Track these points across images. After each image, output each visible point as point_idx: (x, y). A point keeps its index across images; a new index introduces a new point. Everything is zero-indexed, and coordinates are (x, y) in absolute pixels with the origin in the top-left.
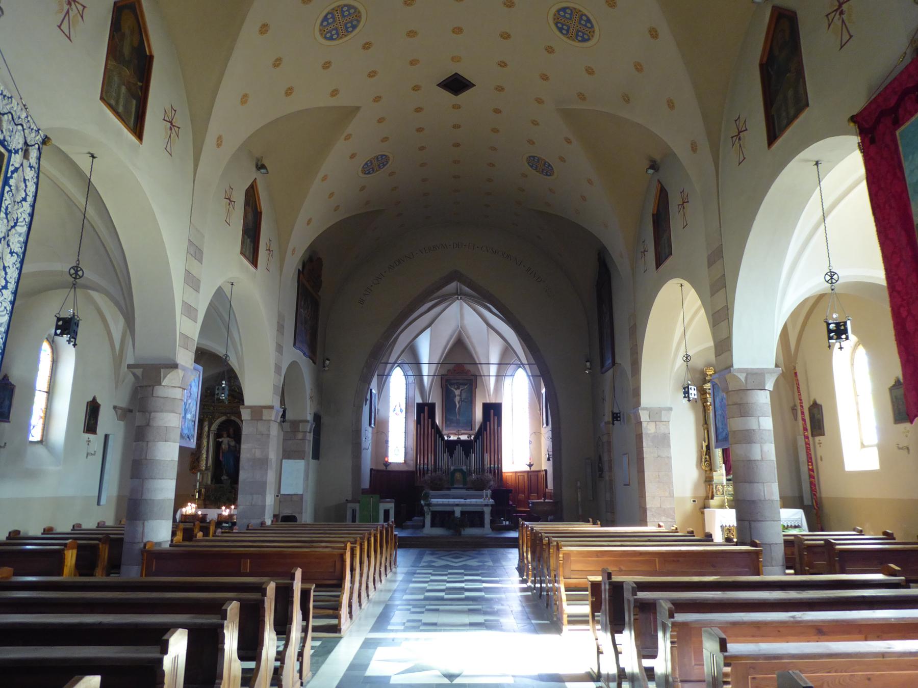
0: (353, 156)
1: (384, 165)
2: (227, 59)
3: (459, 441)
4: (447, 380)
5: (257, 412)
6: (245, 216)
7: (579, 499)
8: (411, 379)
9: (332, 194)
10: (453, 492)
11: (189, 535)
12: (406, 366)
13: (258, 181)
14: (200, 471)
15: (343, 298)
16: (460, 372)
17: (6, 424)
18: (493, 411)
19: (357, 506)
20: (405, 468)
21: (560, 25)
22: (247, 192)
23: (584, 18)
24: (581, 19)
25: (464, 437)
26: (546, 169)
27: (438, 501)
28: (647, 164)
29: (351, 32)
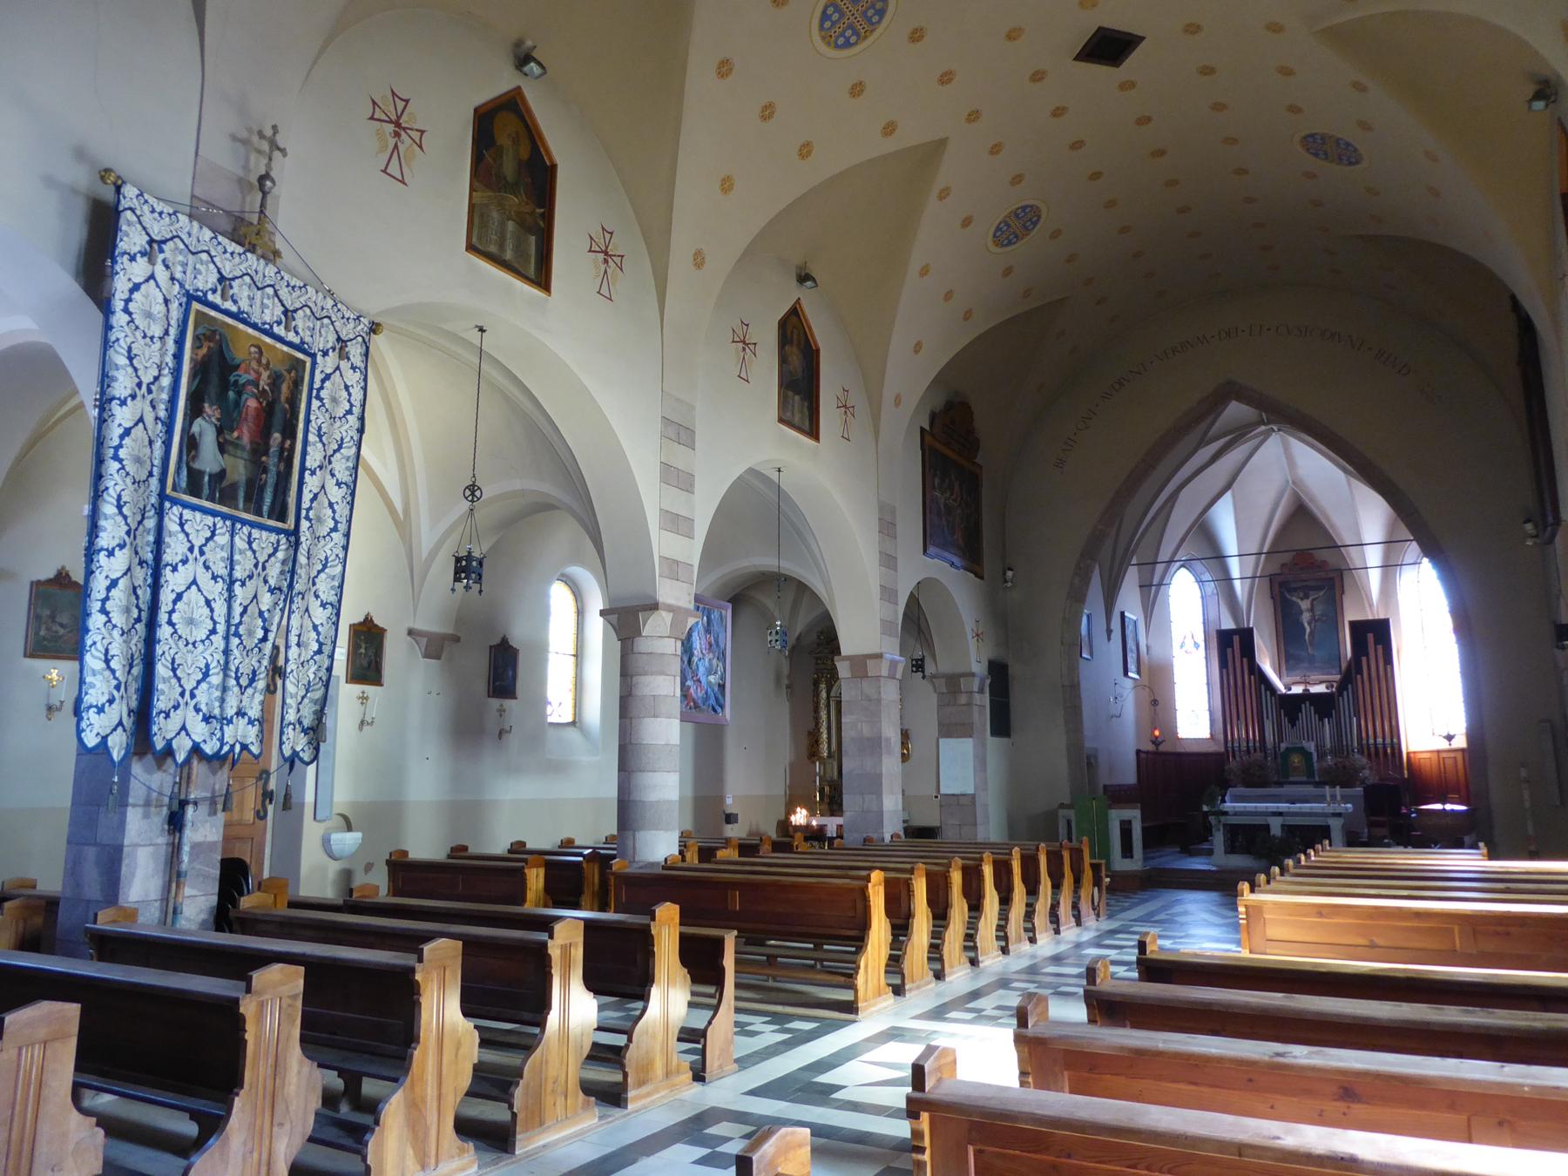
1: (1035, 224)
3: (1306, 696)
4: (1281, 585)
5: (860, 663)
6: (783, 360)
7: (1527, 804)
8: (1210, 587)
10: (1287, 790)
11: (706, 854)
12: (1198, 565)
13: (803, 302)
14: (821, 759)
15: (1022, 463)
16: (1304, 569)
17: (513, 702)
18: (1375, 636)
19: (1071, 814)
20: (1213, 748)
22: (783, 324)
25: (1315, 689)
26: (1345, 154)
27: (1238, 806)
29: (879, 22)
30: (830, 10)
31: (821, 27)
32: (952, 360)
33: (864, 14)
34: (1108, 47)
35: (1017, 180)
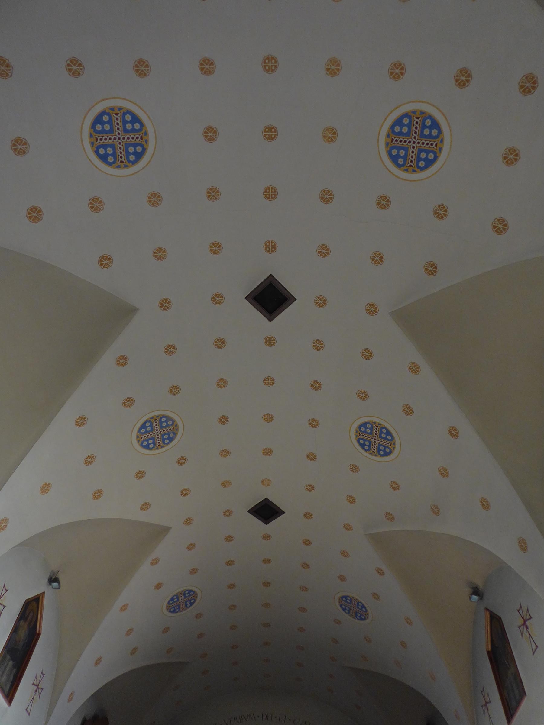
0: (159, 586)
1: (192, 604)
2: (36, 440)
6: (15, 630)
9: (130, 632)
21: (362, 442)
23: (384, 431)
24: (381, 432)
28: (468, 590)
29: (168, 444)
30: (148, 424)
31: (139, 431)
32: (106, 685)
33: (163, 435)
34: (266, 511)
35: (194, 571)
